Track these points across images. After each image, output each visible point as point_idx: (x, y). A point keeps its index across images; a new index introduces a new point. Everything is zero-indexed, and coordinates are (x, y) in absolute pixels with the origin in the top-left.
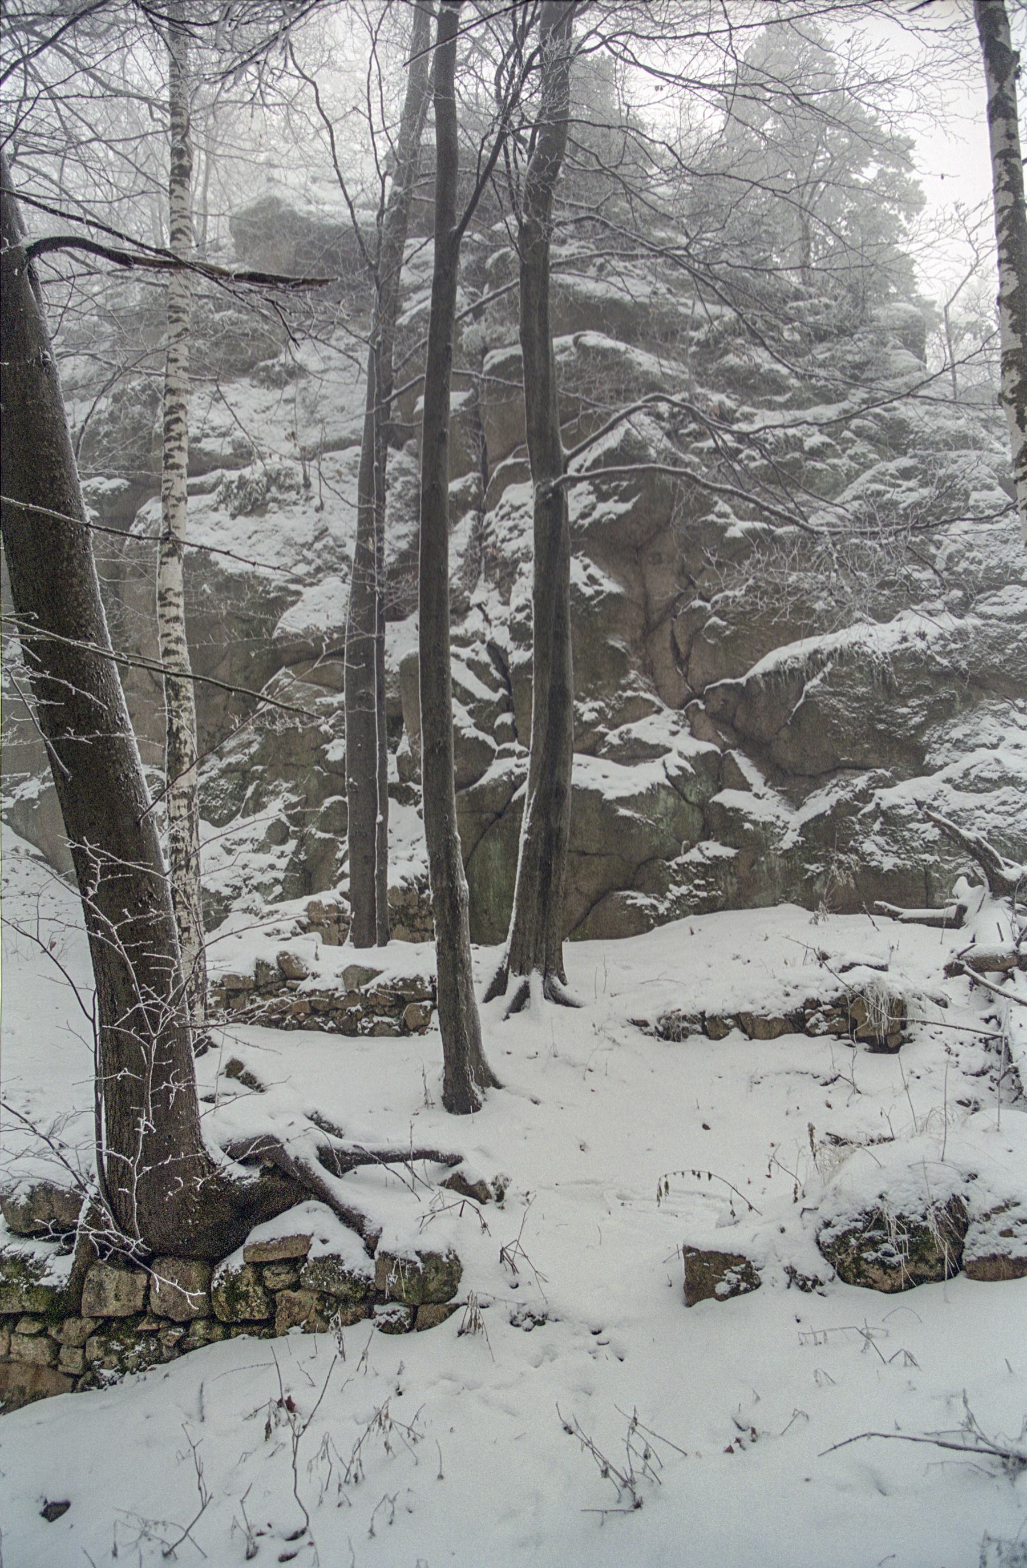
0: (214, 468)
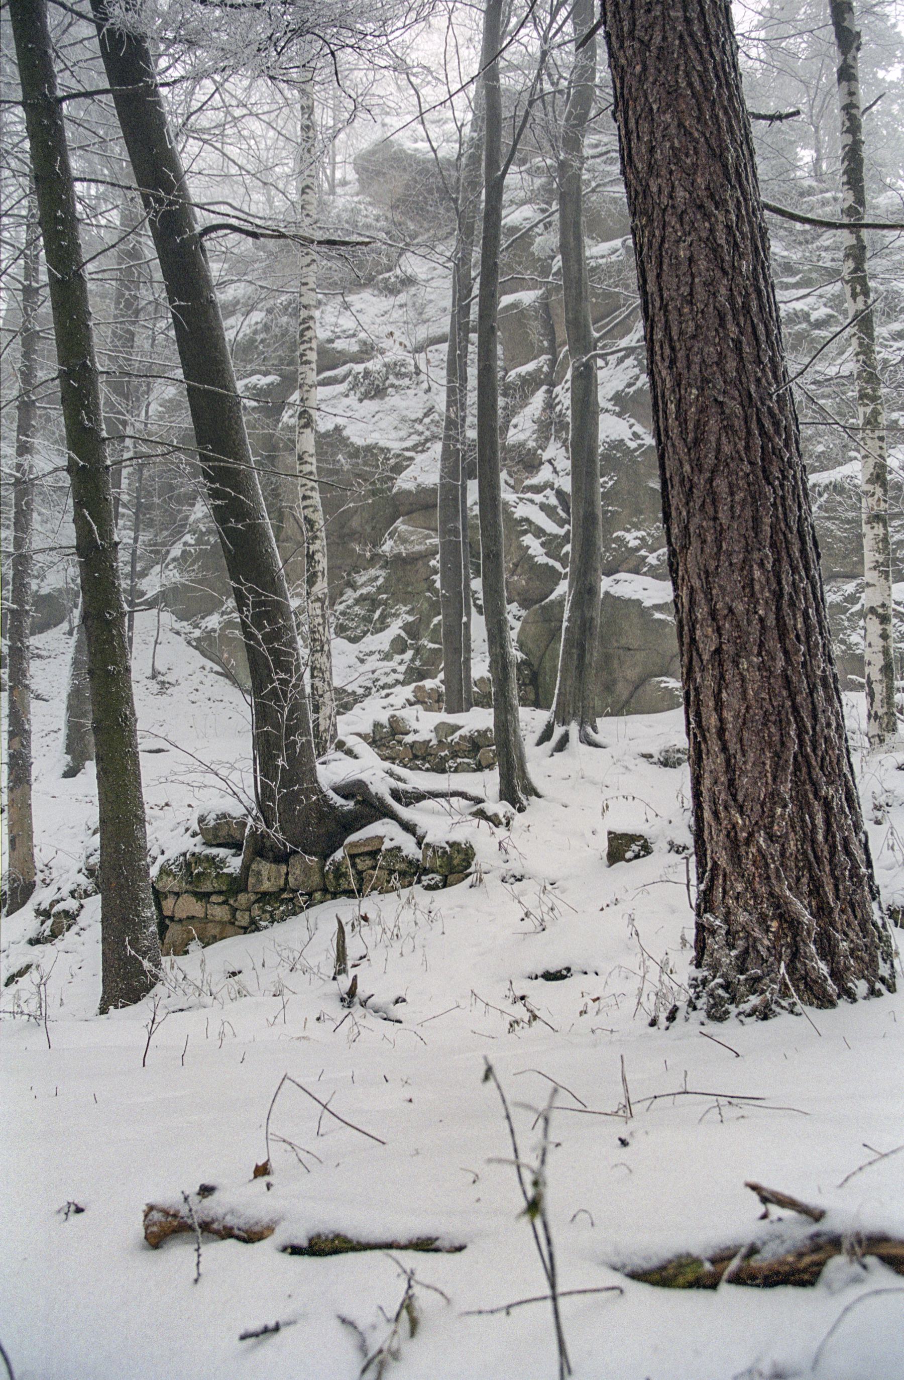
0: (345, 363)
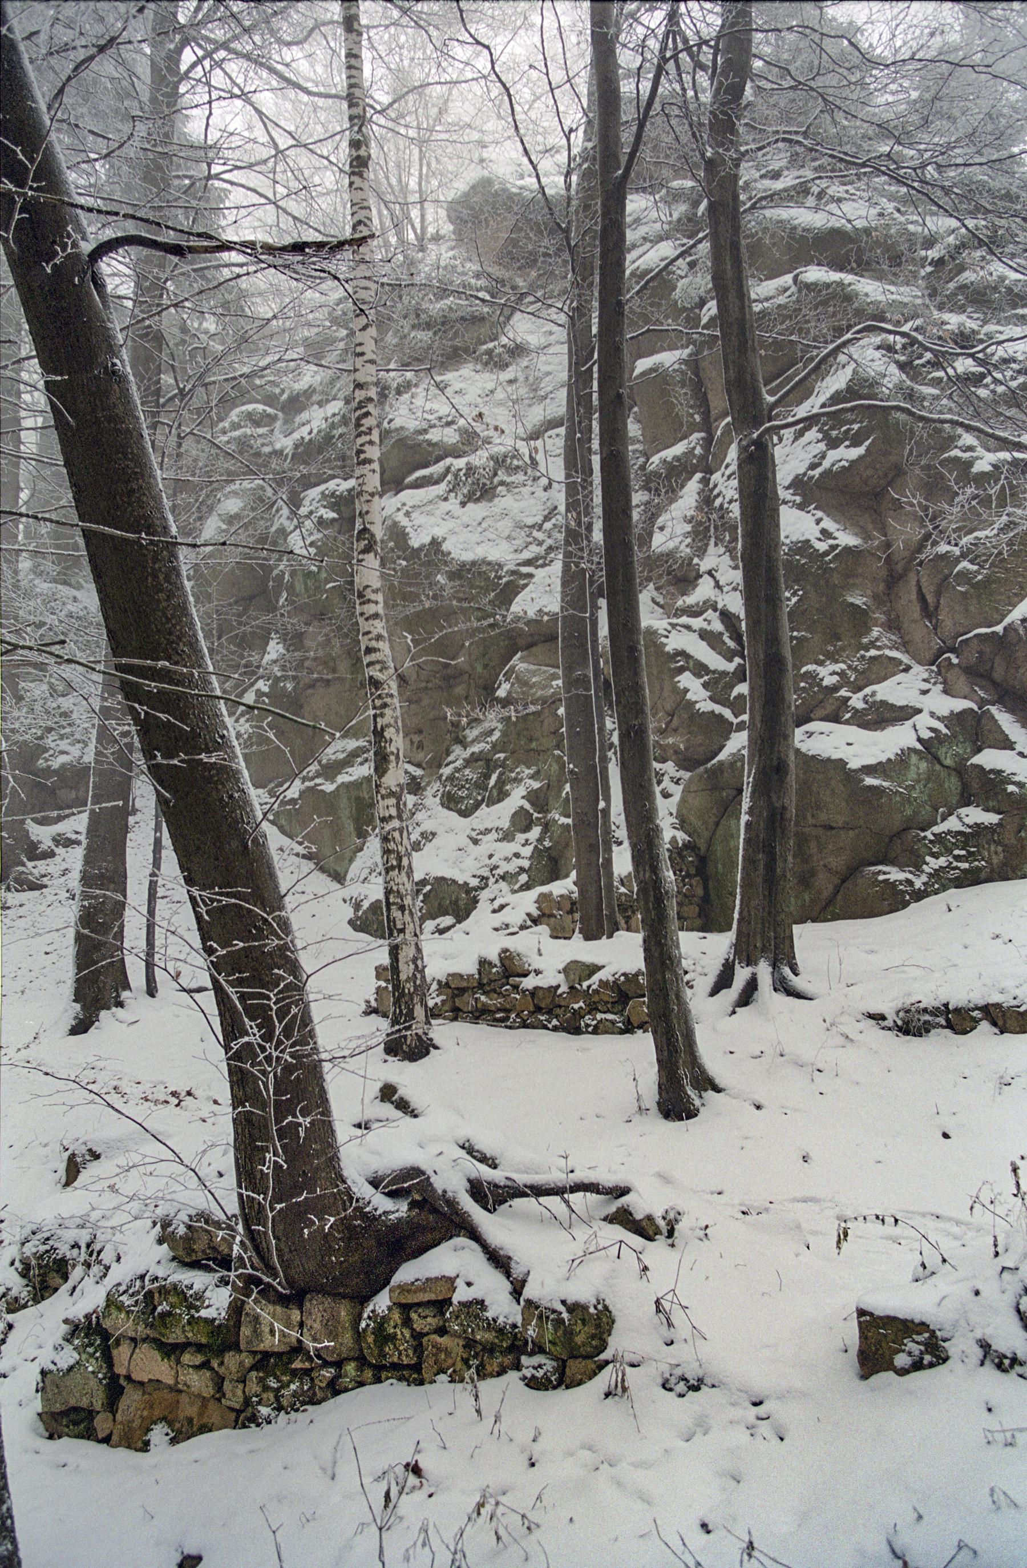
0: (438, 460)
